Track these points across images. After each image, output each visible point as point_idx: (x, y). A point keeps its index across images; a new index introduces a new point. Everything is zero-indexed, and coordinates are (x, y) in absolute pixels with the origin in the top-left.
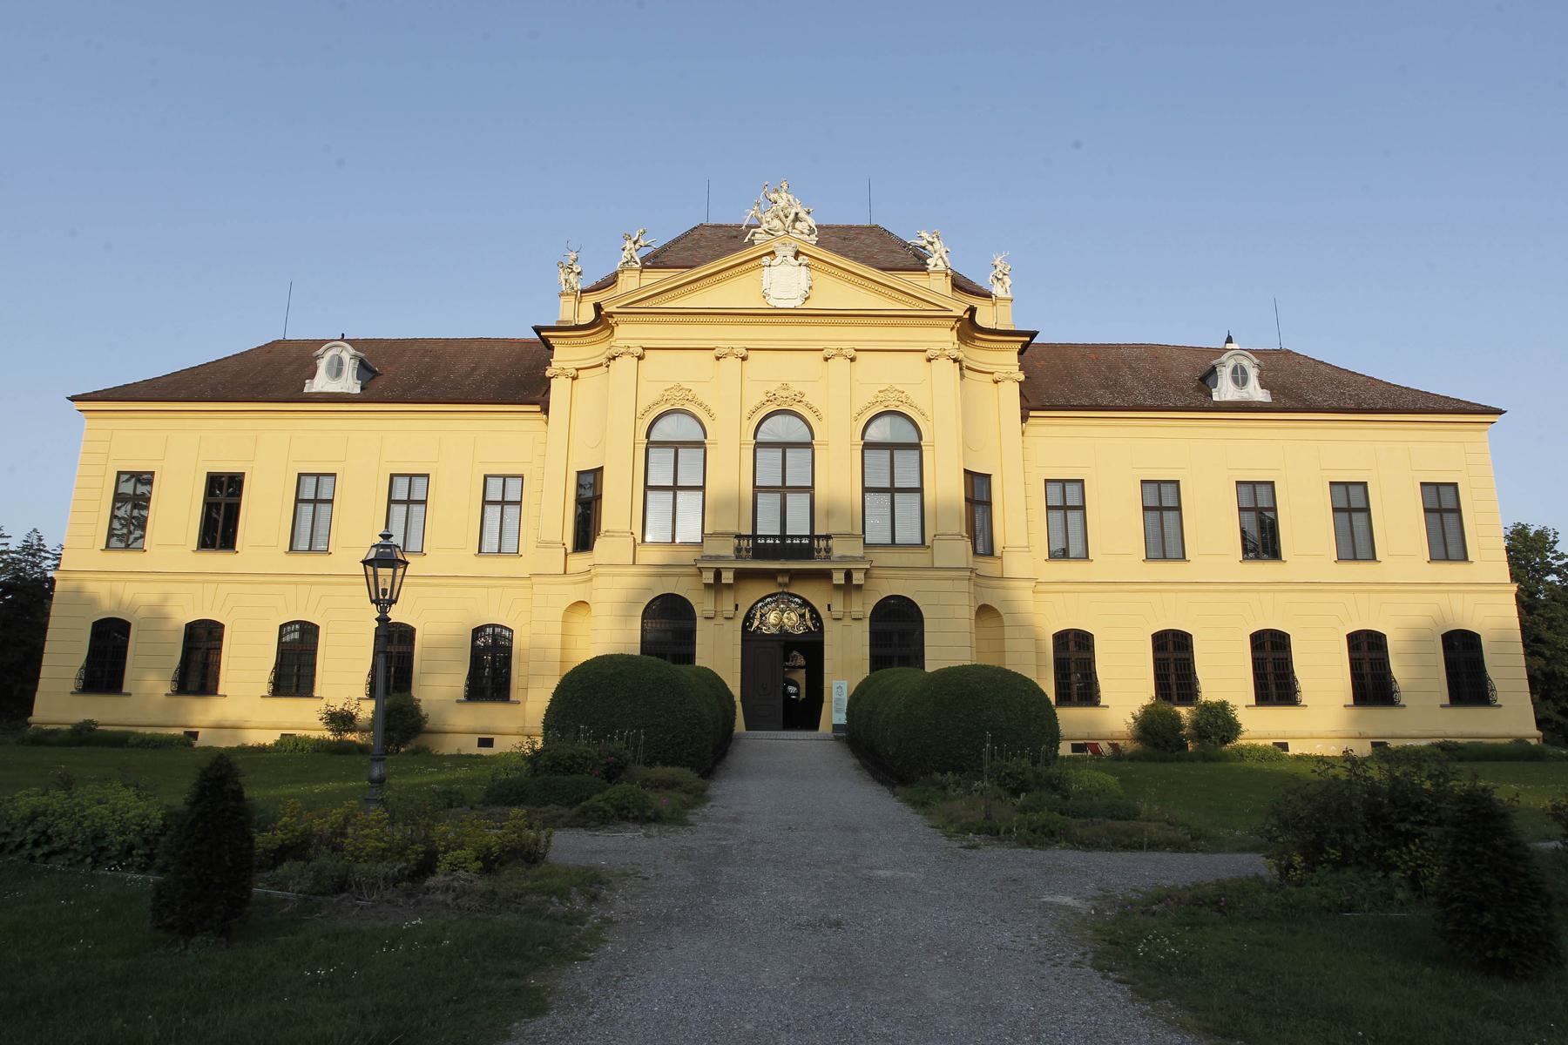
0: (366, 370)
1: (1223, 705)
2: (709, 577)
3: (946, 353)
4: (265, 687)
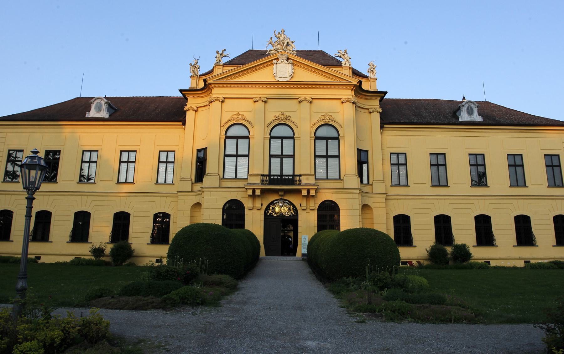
0: (110, 107)
1: (464, 246)
2: (250, 192)
3: (350, 100)
4: (68, 239)
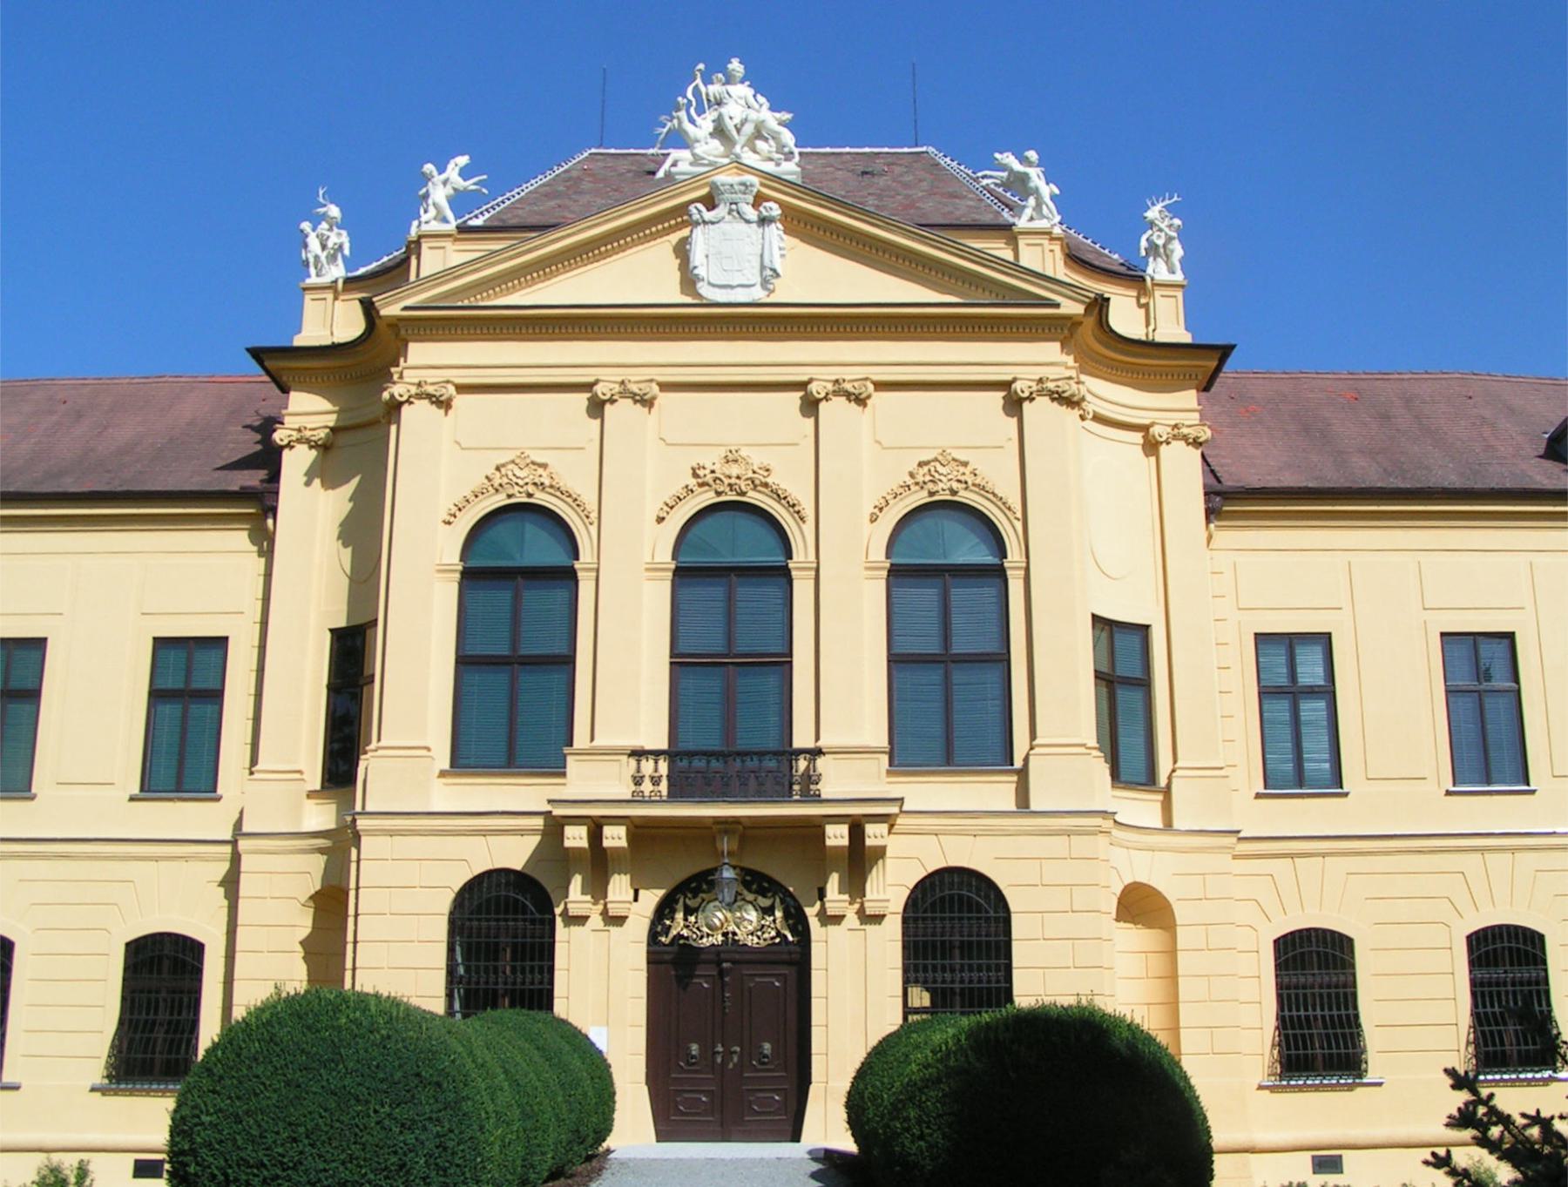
4: (97, 1071)
